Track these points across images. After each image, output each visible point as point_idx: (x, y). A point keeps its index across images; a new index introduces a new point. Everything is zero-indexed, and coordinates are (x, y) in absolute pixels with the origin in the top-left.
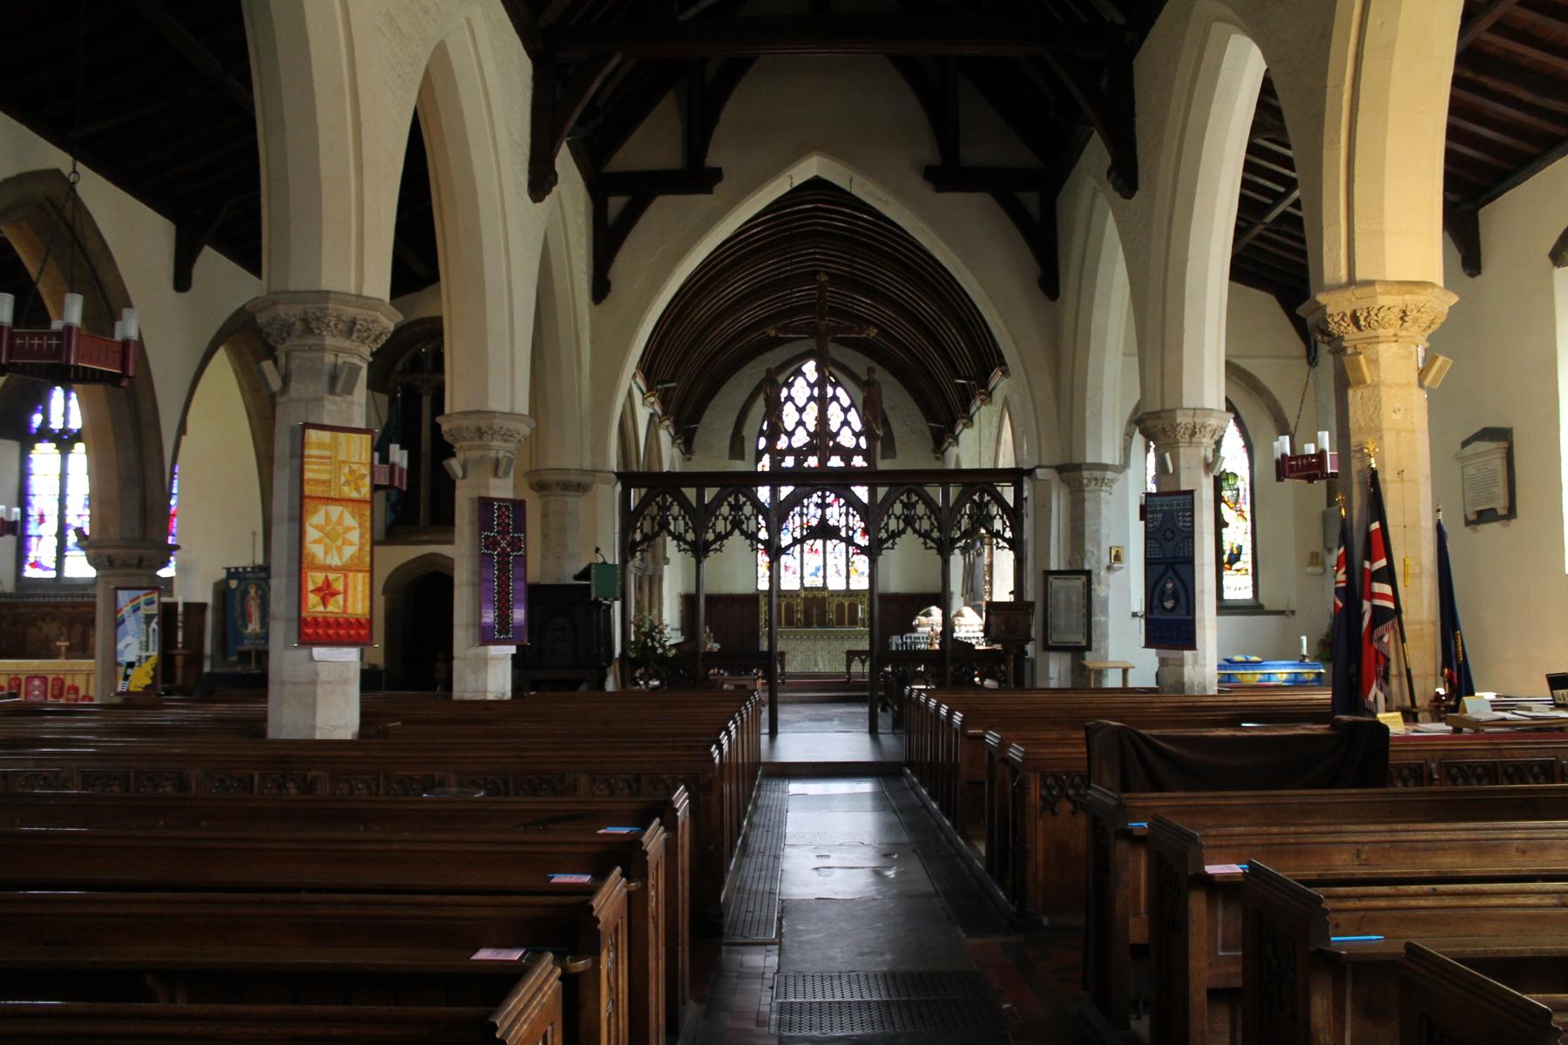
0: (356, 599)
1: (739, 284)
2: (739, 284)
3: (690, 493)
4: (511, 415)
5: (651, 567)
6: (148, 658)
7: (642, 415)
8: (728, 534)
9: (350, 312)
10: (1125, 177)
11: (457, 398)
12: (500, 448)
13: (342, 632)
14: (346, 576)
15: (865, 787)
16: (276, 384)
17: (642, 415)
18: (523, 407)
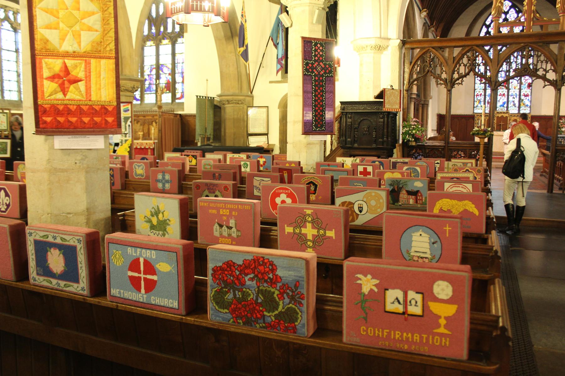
5: (423, 99)
6: (126, 141)
13: (74, 119)
14: (88, 64)
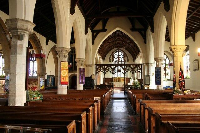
0: (67, 80)
1: (110, 41)
2: (110, 41)
3: (103, 67)
4: (83, 59)
7: (98, 57)
8: (108, 71)
9: (66, 50)
10: (153, 31)
11: (77, 57)
12: (81, 62)
15: (123, 100)
16: (58, 57)
17: (98, 57)
18: (84, 58)
